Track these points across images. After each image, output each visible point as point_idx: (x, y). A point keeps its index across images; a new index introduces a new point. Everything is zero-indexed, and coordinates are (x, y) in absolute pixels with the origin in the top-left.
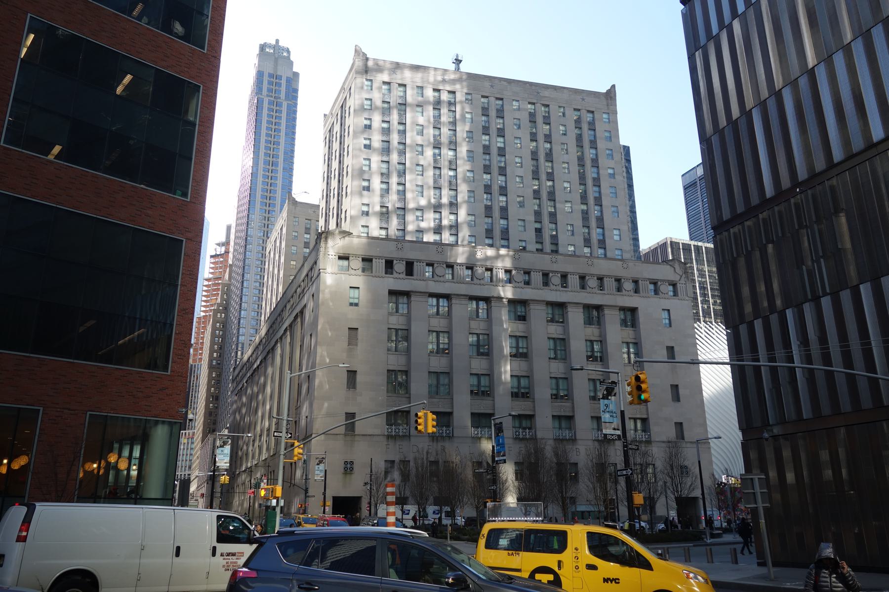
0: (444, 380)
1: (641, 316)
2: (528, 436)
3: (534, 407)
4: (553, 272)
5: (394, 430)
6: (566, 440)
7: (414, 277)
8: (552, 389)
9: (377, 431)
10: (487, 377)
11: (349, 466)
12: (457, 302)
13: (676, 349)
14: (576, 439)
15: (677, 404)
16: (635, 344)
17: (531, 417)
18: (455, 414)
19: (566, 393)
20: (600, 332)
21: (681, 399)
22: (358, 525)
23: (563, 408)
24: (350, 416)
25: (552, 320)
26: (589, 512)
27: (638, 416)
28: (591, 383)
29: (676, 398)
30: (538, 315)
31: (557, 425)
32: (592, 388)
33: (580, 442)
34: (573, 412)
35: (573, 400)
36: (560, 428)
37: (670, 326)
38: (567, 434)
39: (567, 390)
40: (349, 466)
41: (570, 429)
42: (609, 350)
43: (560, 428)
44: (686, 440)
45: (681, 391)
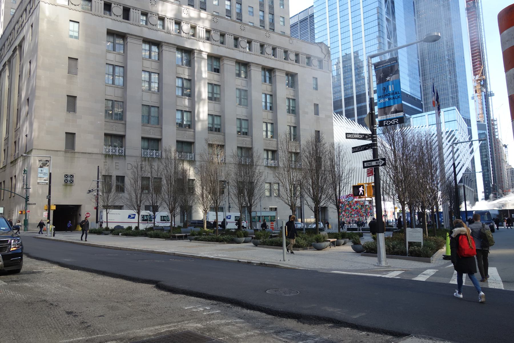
1: (300, 78)
3: (225, 139)
4: (242, 37)
7: (131, 22)
9: (96, 151)
10: (218, 118)
12: (167, 49)
13: (320, 106)
14: (125, 156)
16: (271, 95)
20: (272, 89)
24: (70, 136)
25: (239, 75)
30: (229, 68)
35: (252, 136)
37: (316, 89)
40: (69, 179)
42: (278, 102)
45: (79, 103)
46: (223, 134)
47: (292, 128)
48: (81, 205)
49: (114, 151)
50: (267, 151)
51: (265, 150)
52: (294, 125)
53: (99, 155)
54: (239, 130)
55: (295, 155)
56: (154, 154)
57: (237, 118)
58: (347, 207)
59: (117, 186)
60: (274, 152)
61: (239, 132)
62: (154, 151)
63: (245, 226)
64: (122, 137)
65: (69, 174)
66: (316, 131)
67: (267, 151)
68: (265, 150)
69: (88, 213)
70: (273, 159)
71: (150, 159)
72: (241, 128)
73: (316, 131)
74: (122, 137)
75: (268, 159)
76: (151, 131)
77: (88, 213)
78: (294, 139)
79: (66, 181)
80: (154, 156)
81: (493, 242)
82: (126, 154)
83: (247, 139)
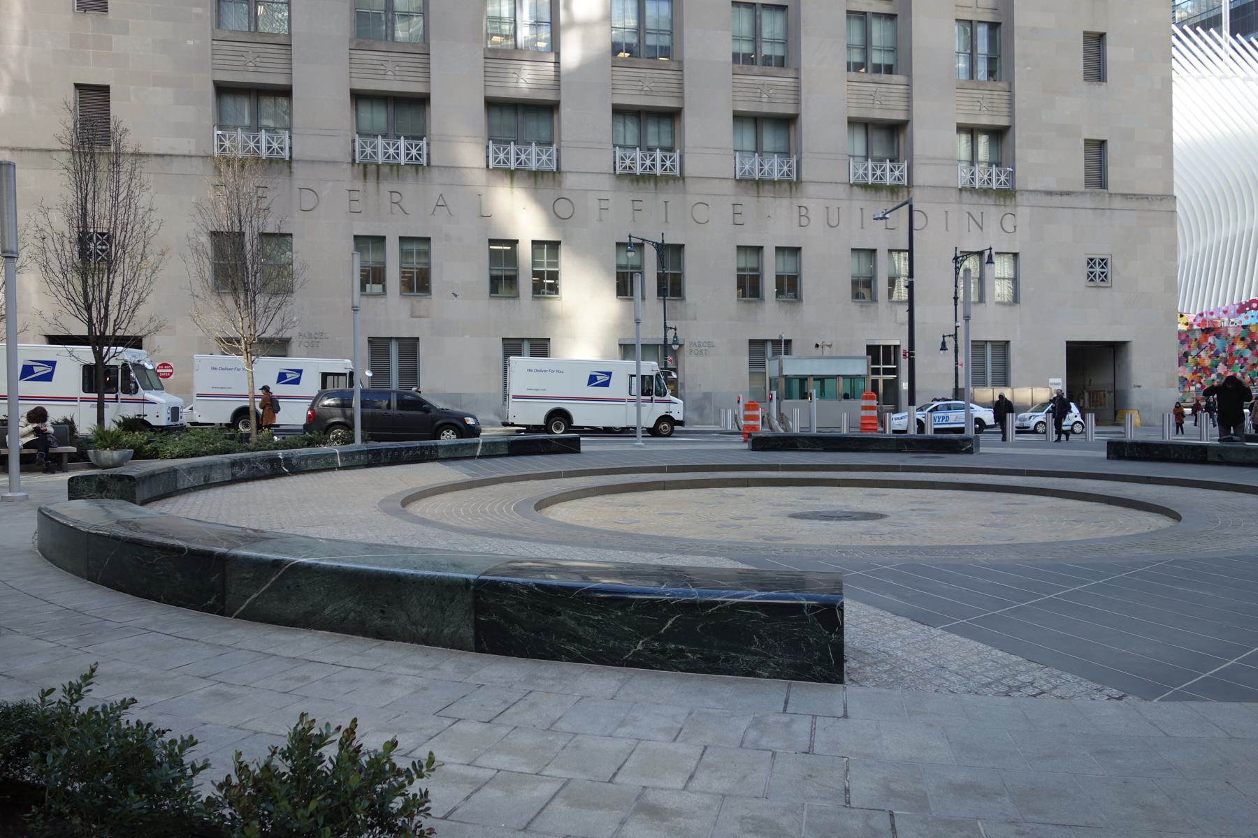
0: (879, 32)
2: (658, 171)
3: (681, 85)
5: (751, 165)
6: (773, 182)
8: (736, 39)
10: (779, 18)
11: (1098, 270)
14: (682, 177)
15: (1096, 88)
17: (671, 116)
18: (806, 121)
19: (779, 51)
21: (1109, 76)
22: (362, 428)
23: (769, 93)
24: (93, 97)
26: (821, 379)
27: (985, 120)
28: (856, 26)
29: (1096, 70)
31: (749, 143)
32: (857, 39)
33: (811, 189)
34: (798, 103)
35: (798, 70)
36: (758, 149)
38: (775, 167)
39: (785, 43)
40: (1098, 270)
41: (786, 154)
43: (758, 149)
44: (1112, 187)
45: (1113, 53)
46: (792, 73)
47: (982, 31)
48: (1124, 344)
49: (523, 157)
50: (971, 131)
51: (961, 129)
52: (989, 18)
53: (195, 161)
54: (857, 57)
55: (990, 141)
56: (403, 152)
57: (850, 13)
58: (1239, 346)
59: (661, 279)
60: (998, 134)
61: (853, 67)
62: (402, 143)
63: (678, 416)
64: (787, 122)
65: (1097, 257)
66: (1088, 36)
67: (971, 131)
68: (961, 129)
69: (164, 365)
70: (996, 162)
71: (385, 170)
72: (866, 47)
73: (1088, 36)
74: (787, 122)
75: (973, 161)
76: (390, 66)
77: (164, 365)
78: (991, 73)
79: (1091, 277)
80: (403, 160)
81: (45, 566)
82: (687, 173)
83: (782, 81)
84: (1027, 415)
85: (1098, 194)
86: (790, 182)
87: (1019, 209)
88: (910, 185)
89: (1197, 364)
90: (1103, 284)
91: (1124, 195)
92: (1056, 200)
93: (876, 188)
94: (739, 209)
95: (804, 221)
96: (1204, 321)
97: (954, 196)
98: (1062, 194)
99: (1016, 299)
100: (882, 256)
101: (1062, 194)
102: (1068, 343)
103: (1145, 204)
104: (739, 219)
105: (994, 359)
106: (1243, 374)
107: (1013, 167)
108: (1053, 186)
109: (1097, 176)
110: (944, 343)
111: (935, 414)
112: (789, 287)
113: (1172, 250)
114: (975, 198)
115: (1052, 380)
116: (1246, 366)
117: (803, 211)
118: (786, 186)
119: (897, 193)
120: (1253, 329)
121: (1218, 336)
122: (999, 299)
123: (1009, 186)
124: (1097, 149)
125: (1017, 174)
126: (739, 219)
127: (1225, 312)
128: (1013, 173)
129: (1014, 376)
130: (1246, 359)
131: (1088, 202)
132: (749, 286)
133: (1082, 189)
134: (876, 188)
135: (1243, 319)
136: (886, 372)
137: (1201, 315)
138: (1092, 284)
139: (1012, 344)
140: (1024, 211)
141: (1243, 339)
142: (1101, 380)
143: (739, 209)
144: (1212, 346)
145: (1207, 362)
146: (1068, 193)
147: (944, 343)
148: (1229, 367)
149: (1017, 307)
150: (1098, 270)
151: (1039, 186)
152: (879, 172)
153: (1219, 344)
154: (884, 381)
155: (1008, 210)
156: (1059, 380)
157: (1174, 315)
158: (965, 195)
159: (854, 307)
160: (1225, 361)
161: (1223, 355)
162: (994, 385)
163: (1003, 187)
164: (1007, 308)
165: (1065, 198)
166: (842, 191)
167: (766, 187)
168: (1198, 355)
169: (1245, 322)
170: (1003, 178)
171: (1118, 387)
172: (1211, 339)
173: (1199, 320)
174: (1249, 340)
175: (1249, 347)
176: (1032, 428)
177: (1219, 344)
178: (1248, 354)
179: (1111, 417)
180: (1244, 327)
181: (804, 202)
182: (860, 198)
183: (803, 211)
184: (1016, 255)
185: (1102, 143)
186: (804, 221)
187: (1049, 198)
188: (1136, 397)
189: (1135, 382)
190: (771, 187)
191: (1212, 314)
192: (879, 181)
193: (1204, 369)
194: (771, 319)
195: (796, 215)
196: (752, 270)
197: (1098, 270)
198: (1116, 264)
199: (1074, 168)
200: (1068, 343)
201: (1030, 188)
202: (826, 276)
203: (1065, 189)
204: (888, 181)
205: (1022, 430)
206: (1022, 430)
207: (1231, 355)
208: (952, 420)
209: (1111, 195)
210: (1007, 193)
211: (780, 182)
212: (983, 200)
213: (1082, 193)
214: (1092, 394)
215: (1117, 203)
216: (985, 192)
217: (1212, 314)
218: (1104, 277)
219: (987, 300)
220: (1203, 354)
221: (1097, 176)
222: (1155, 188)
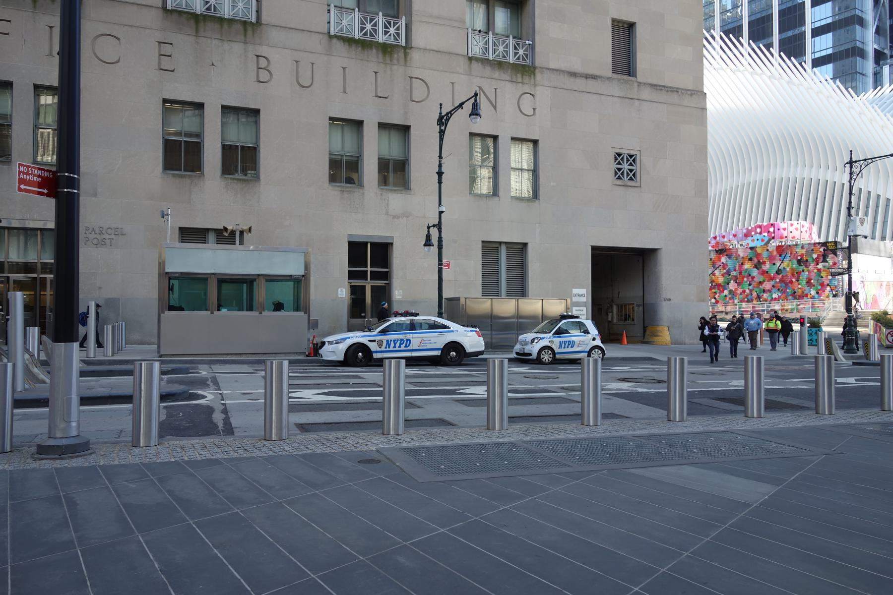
6: (221, 20)
33: (274, 35)
40: (625, 167)
44: (640, 77)
48: (653, 251)
58: (747, 266)
65: (626, 152)
79: (618, 174)
84: (529, 336)
85: (626, 82)
86: (245, 24)
87: (538, 88)
88: (408, 47)
89: (712, 282)
90: (631, 183)
91: (654, 86)
92: (580, 83)
93: (364, 44)
94: (167, 49)
95: (264, 76)
96: (717, 243)
97: (463, 64)
98: (587, 77)
99: (536, 195)
100: (370, 132)
101: (587, 77)
102: (594, 248)
103: (675, 98)
104: (166, 63)
105: (507, 264)
106: (751, 291)
107: (533, 41)
108: (578, 68)
109: (625, 61)
110: (428, 237)
111: (391, 337)
112: (241, 161)
113: (702, 150)
114: (488, 70)
115: (575, 291)
116: (754, 284)
117: (263, 63)
118: (239, 27)
119: (391, 53)
120: (759, 250)
121: (729, 256)
122: (513, 194)
123: (528, 62)
124: (625, 32)
125: (537, 49)
126: (166, 63)
127: (735, 236)
128: (532, 47)
129: (533, 284)
130: (753, 278)
131: (615, 89)
132: (181, 156)
133: (609, 73)
134: (364, 44)
135: (749, 242)
136: (375, 276)
137: (715, 238)
138: (619, 182)
139: (530, 246)
140: (544, 92)
141: (750, 259)
142: (630, 293)
143: (167, 49)
144: (724, 266)
145: (721, 280)
146: (594, 77)
147: (428, 237)
148: (739, 284)
149: (536, 204)
150: (626, 167)
151: (563, 66)
152: (369, 27)
153: (730, 264)
154: (363, 288)
155: (527, 89)
156: (583, 291)
157: (702, 224)
158: (475, 65)
159: (333, 193)
160: (736, 279)
161: (734, 273)
162: (510, 295)
163: (521, 62)
164: (524, 205)
165: (591, 82)
166: (317, 43)
167: (210, 25)
168: (713, 274)
169: (752, 245)
170: (521, 52)
171: (648, 300)
172: (724, 259)
173: (713, 242)
174: (755, 260)
175: (756, 267)
176: (534, 356)
177: (730, 264)
178: (755, 272)
179: (640, 334)
180: (752, 248)
181: (264, 50)
182: (342, 56)
183: (263, 63)
184: (535, 142)
185: (631, 26)
186: (264, 76)
187: (572, 79)
188: (666, 312)
189: (665, 294)
190: (217, 26)
191: (724, 237)
192: (368, 38)
193: (719, 285)
194: (212, 198)
195: (253, 67)
196: (190, 135)
197: (626, 167)
198: (645, 163)
199: (600, 51)
200: (594, 248)
201: (552, 66)
202: (294, 151)
203: (590, 71)
204: (381, 38)
205: (523, 359)
206: (523, 359)
207: (740, 273)
208: (414, 345)
209: (639, 84)
210: (525, 69)
211: (231, 21)
212: (497, 74)
213: (609, 79)
214: (621, 307)
215: (646, 94)
216: (500, 65)
217: (724, 237)
218: (633, 176)
219: (501, 193)
220: (717, 272)
221: (625, 61)
222: (686, 83)
